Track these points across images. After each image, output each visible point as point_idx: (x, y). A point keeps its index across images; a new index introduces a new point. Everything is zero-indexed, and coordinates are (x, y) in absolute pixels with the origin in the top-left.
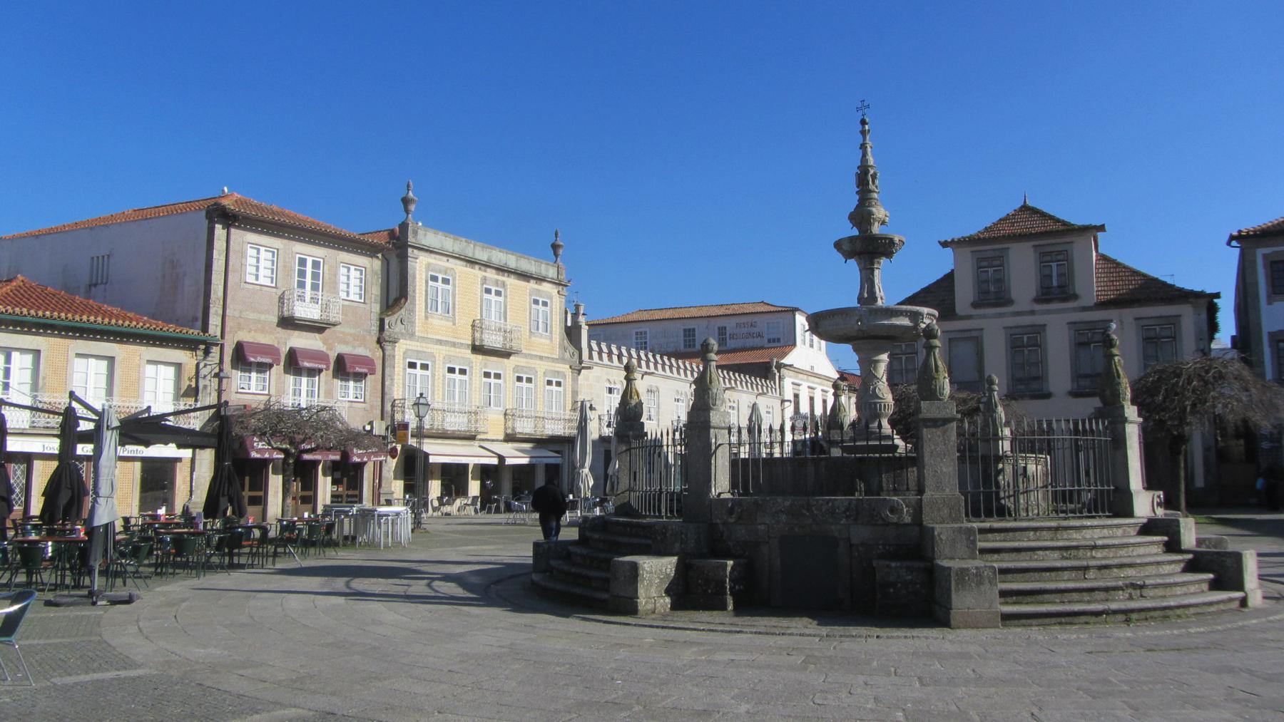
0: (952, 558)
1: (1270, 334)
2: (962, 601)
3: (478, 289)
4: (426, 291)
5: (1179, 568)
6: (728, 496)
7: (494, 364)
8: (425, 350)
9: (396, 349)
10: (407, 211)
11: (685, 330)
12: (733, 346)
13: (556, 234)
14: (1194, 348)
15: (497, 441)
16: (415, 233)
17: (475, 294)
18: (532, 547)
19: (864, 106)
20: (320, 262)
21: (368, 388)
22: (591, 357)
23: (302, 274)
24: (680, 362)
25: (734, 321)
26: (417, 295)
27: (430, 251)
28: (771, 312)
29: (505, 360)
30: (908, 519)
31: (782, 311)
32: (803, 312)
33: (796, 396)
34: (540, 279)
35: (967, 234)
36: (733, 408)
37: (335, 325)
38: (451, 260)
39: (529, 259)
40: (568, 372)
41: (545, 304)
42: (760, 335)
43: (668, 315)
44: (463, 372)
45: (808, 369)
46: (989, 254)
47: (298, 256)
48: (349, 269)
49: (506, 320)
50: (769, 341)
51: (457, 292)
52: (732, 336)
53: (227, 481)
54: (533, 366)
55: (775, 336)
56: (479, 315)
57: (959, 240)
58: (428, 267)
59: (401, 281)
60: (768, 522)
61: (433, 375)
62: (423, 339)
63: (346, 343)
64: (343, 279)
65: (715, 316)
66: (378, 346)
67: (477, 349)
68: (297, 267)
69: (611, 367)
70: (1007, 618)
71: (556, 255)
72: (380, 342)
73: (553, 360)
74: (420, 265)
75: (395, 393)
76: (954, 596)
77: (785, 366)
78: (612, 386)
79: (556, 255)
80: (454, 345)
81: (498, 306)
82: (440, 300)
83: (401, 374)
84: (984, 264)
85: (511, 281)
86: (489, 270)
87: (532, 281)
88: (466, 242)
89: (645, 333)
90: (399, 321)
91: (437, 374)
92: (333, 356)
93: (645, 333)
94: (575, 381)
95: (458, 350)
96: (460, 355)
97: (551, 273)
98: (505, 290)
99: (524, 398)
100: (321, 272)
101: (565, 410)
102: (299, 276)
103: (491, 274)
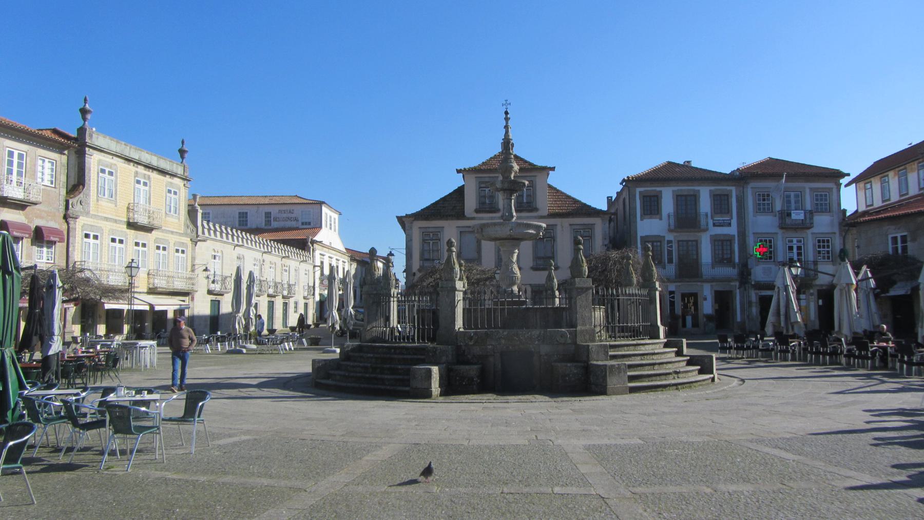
0: (597, 361)
1: (641, 237)
2: (612, 382)
3: (132, 180)
4: (98, 181)
5: (684, 363)
6: (462, 330)
7: (142, 237)
8: (96, 225)
9: (77, 224)
10: (85, 119)
11: (240, 213)
12: (276, 226)
13: (183, 142)
14: (601, 243)
15: (143, 293)
16: (91, 136)
17: (130, 184)
18: (311, 362)
19: (507, 103)
20: (23, 155)
21: (57, 252)
22: (203, 233)
23: (10, 163)
24: (257, 237)
25: (277, 208)
26: (92, 183)
27: (101, 150)
28: (305, 204)
29: (149, 234)
30: (569, 341)
31: (312, 203)
32: (327, 204)
33: (322, 263)
34: (173, 175)
35: (472, 165)
36: (286, 271)
37: (36, 204)
38: (114, 158)
39: (165, 159)
40: (189, 243)
41: (175, 193)
42: (296, 220)
43: (226, 201)
44: (121, 242)
45: (328, 244)
46: (487, 180)
47: (8, 149)
48: (44, 161)
49: (150, 204)
50: (303, 224)
51: (118, 182)
52: (275, 219)
53: (38, 324)
54: (167, 238)
55: (307, 221)
56: (132, 199)
57: (469, 170)
58: (99, 162)
59: (79, 172)
60: (493, 344)
61: (102, 244)
62: (95, 217)
63: (42, 218)
64: (40, 169)
65: (263, 204)
66: (64, 221)
67: (132, 225)
68: (7, 158)
69: (216, 240)
70: (633, 390)
71: (182, 157)
72: (66, 217)
73: (180, 234)
74: (93, 160)
75: (76, 256)
76: (608, 380)
77: (316, 242)
78: (216, 254)
79: (182, 157)
80: (116, 221)
81: (145, 193)
82: (106, 188)
83: (80, 242)
84: (483, 185)
85: (154, 175)
86: (139, 166)
87: (167, 176)
88: (125, 145)
89: (209, 213)
90: (79, 202)
91: (104, 243)
92: (33, 227)
93: (209, 213)
94: (193, 250)
95: (118, 225)
96: (119, 229)
97: (180, 171)
98: (150, 182)
99: (161, 261)
100: (24, 162)
101: (187, 271)
102: (8, 165)
103: (141, 169)
